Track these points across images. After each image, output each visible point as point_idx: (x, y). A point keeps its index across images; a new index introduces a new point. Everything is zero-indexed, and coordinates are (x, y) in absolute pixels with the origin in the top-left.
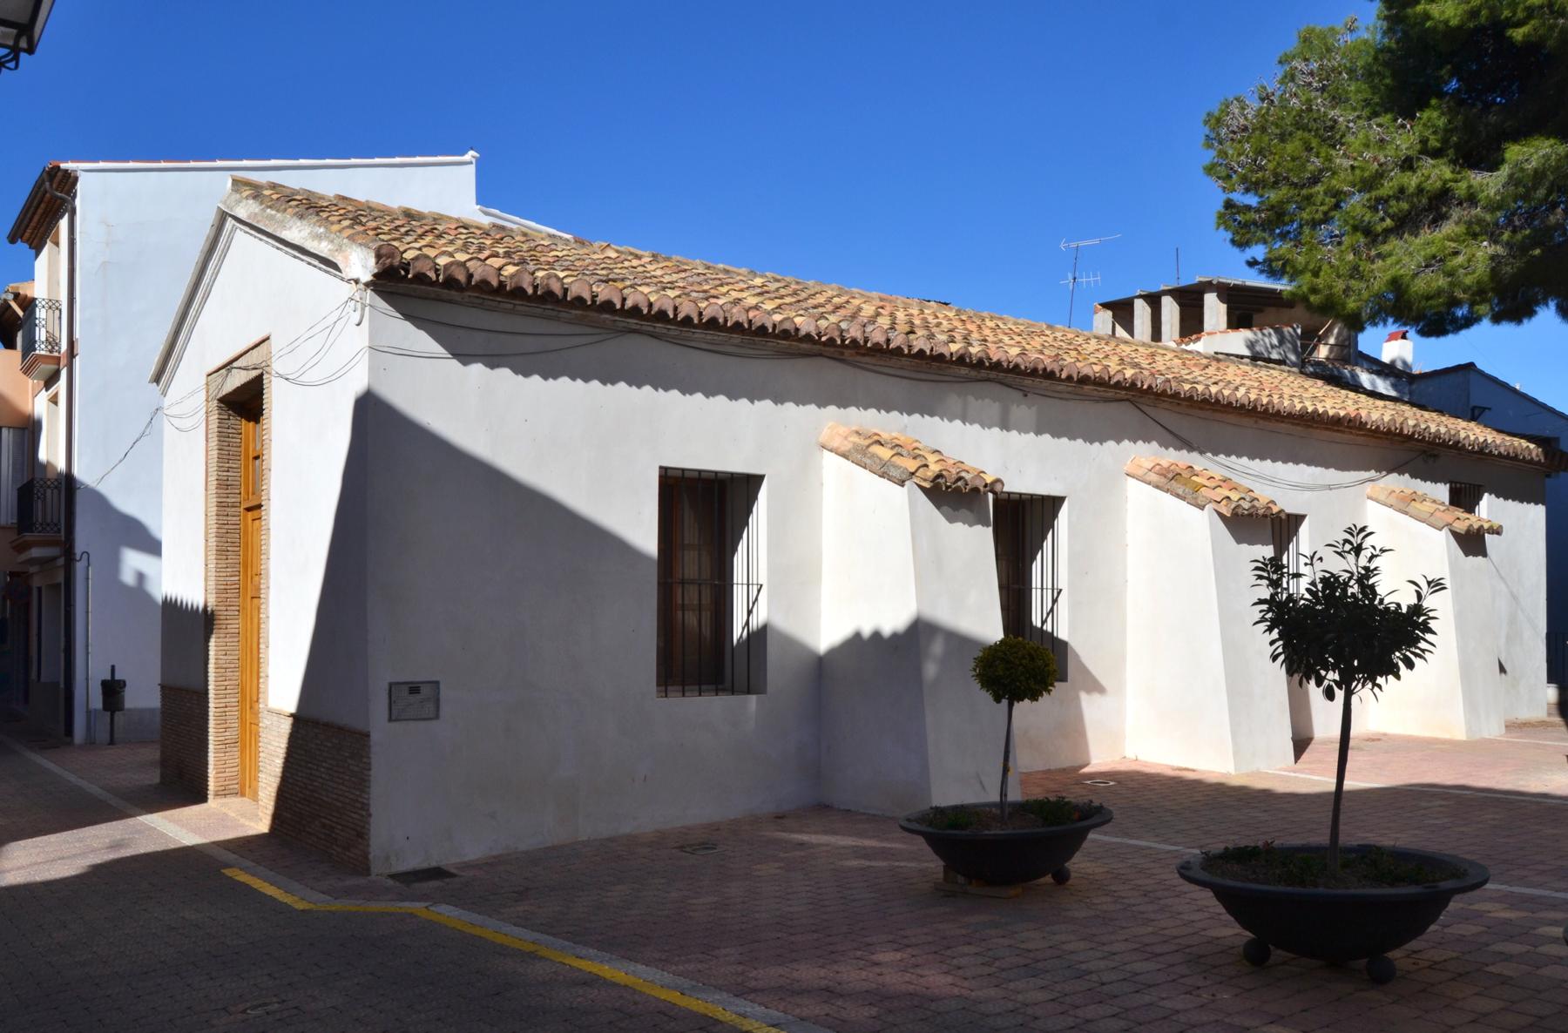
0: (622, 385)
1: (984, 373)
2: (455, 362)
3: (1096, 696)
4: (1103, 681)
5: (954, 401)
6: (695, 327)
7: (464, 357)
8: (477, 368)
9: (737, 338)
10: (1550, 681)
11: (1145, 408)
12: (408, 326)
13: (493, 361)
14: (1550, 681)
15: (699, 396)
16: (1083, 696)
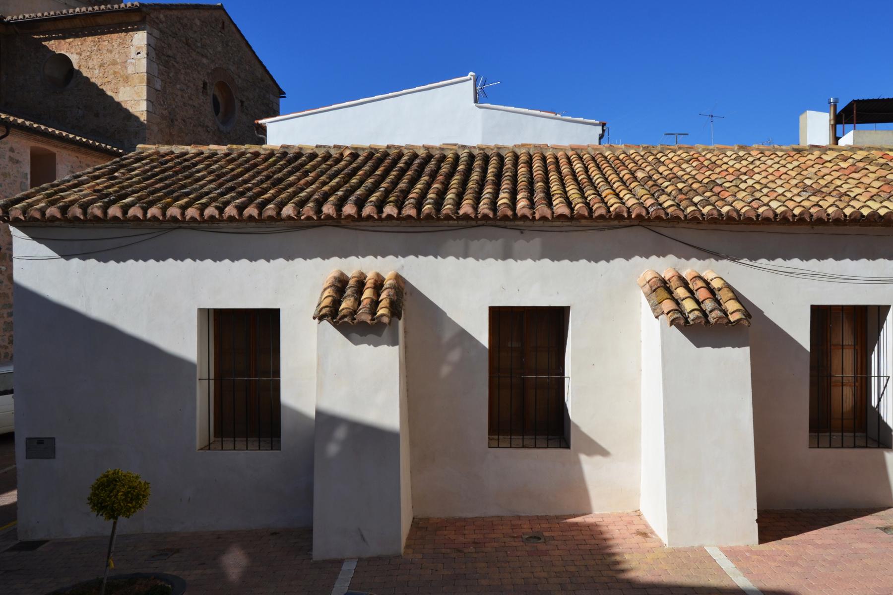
0: (171, 260)
1: (480, 222)
2: (63, 260)
3: (598, 459)
4: (609, 450)
5: (475, 245)
6: (683, 221)
7: (67, 256)
8: (75, 261)
9: (855, 229)
10: (269, 261)
11: (657, 229)
12: (35, 243)
13: (84, 256)
14: (269, 261)
15: (227, 261)
16: (583, 458)
